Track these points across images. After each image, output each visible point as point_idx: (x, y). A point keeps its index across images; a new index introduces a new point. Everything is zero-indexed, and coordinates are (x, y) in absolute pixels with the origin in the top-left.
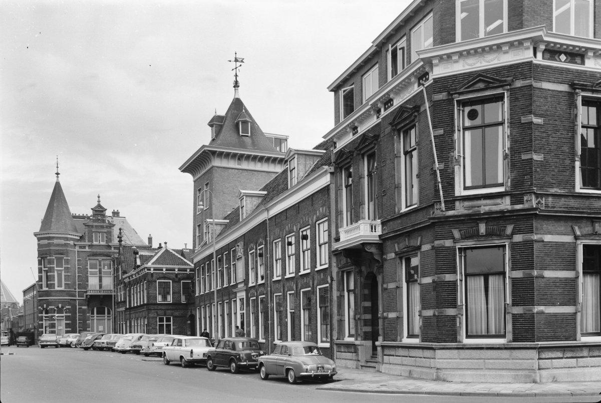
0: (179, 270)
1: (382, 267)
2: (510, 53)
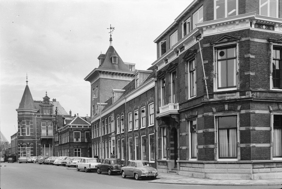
0: (84, 127)
1: (179, 125)
2: (239, 25)
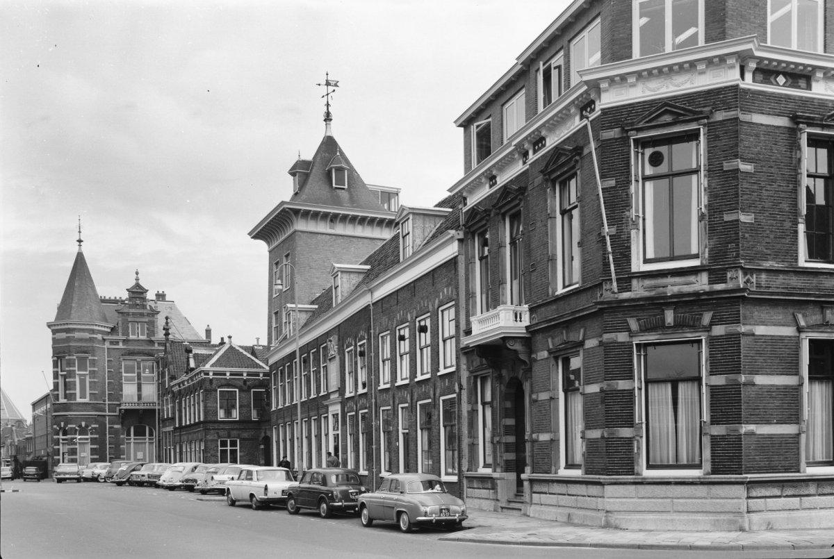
0: (249, 374)
1: (530, 370)
2: (708, 73)
